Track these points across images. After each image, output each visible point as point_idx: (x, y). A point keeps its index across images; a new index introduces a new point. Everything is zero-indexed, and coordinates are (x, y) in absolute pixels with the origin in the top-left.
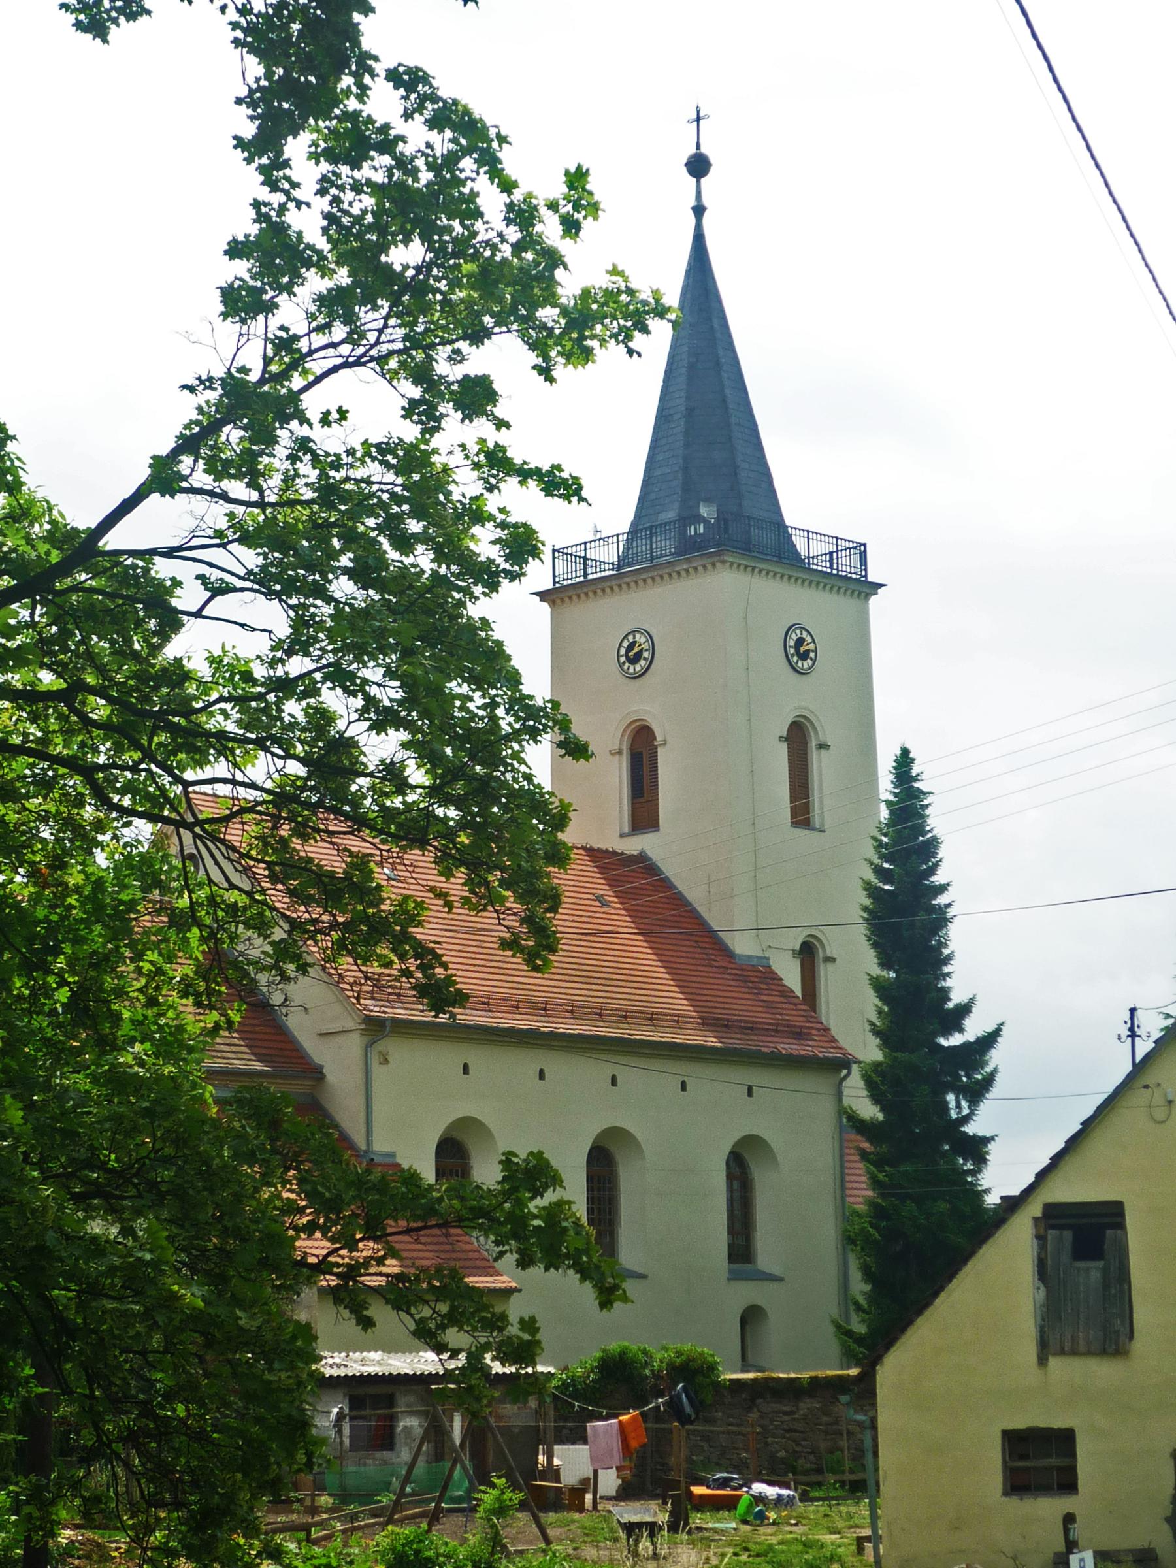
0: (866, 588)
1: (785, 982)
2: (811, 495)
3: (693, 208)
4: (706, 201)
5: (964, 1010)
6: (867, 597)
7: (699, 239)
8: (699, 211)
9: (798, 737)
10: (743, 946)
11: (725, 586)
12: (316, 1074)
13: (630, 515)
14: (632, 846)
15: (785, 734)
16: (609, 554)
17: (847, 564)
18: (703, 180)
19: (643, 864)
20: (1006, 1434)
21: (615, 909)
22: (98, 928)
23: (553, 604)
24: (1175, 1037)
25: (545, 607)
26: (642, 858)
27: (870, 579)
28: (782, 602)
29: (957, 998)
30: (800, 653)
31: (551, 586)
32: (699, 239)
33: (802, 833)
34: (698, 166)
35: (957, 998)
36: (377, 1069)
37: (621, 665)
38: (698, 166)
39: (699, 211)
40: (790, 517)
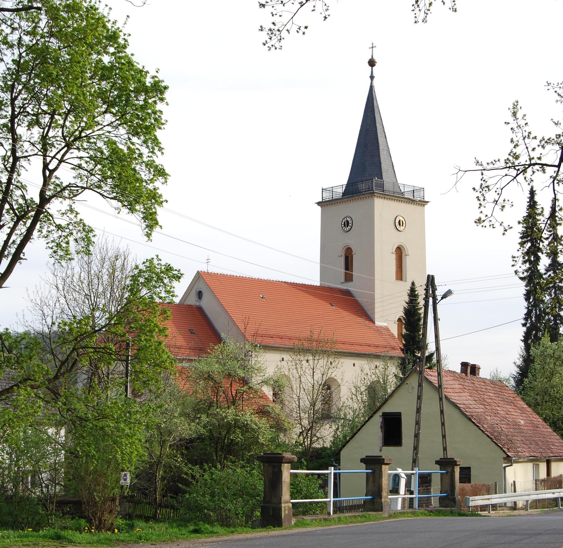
0: (423, 203)
1: (392, 331)
3: (198, 272)
4: (374, 74)
6: (424, 205)
7: (372, 87)
8: (372, 77)
9: (400, 252)
13: (345, 181)
14: (344, 287)
16: (341, 191)
18: (374, 68)
19: (348, 293)
20: (399, 414)
21: (557, 446)
22: (63, 452)
23: (321, 206)
25: (319, 208)
31: (321, 200)
32: (372, 87)
33: (400, 282)
37: (342, 228)
38: (372, 63)
39: (372, 77)
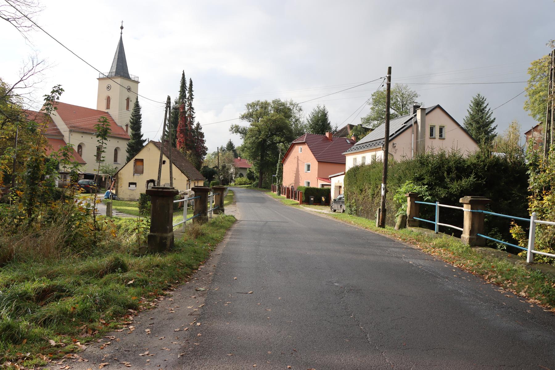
2: (132, 71)
5: (142, 136)
7: (121, 37)
8: (121, 33)
10: (119, 124)
11: (119, 80)
12: (63, 136)
14: (106, 111)
15: (63, 99)
17: (136, 79)
24: (2, 266)
26: (107, 113)
27: (384, 136)
28: (127, 83)
29: (142, 134)
30: (129, 89)
32: (121, 37)
34: (122, 28)
35: (142, 134)
36: (71, 136)
38: (122, 28)
39: (121, 33)
40: (129, 73)
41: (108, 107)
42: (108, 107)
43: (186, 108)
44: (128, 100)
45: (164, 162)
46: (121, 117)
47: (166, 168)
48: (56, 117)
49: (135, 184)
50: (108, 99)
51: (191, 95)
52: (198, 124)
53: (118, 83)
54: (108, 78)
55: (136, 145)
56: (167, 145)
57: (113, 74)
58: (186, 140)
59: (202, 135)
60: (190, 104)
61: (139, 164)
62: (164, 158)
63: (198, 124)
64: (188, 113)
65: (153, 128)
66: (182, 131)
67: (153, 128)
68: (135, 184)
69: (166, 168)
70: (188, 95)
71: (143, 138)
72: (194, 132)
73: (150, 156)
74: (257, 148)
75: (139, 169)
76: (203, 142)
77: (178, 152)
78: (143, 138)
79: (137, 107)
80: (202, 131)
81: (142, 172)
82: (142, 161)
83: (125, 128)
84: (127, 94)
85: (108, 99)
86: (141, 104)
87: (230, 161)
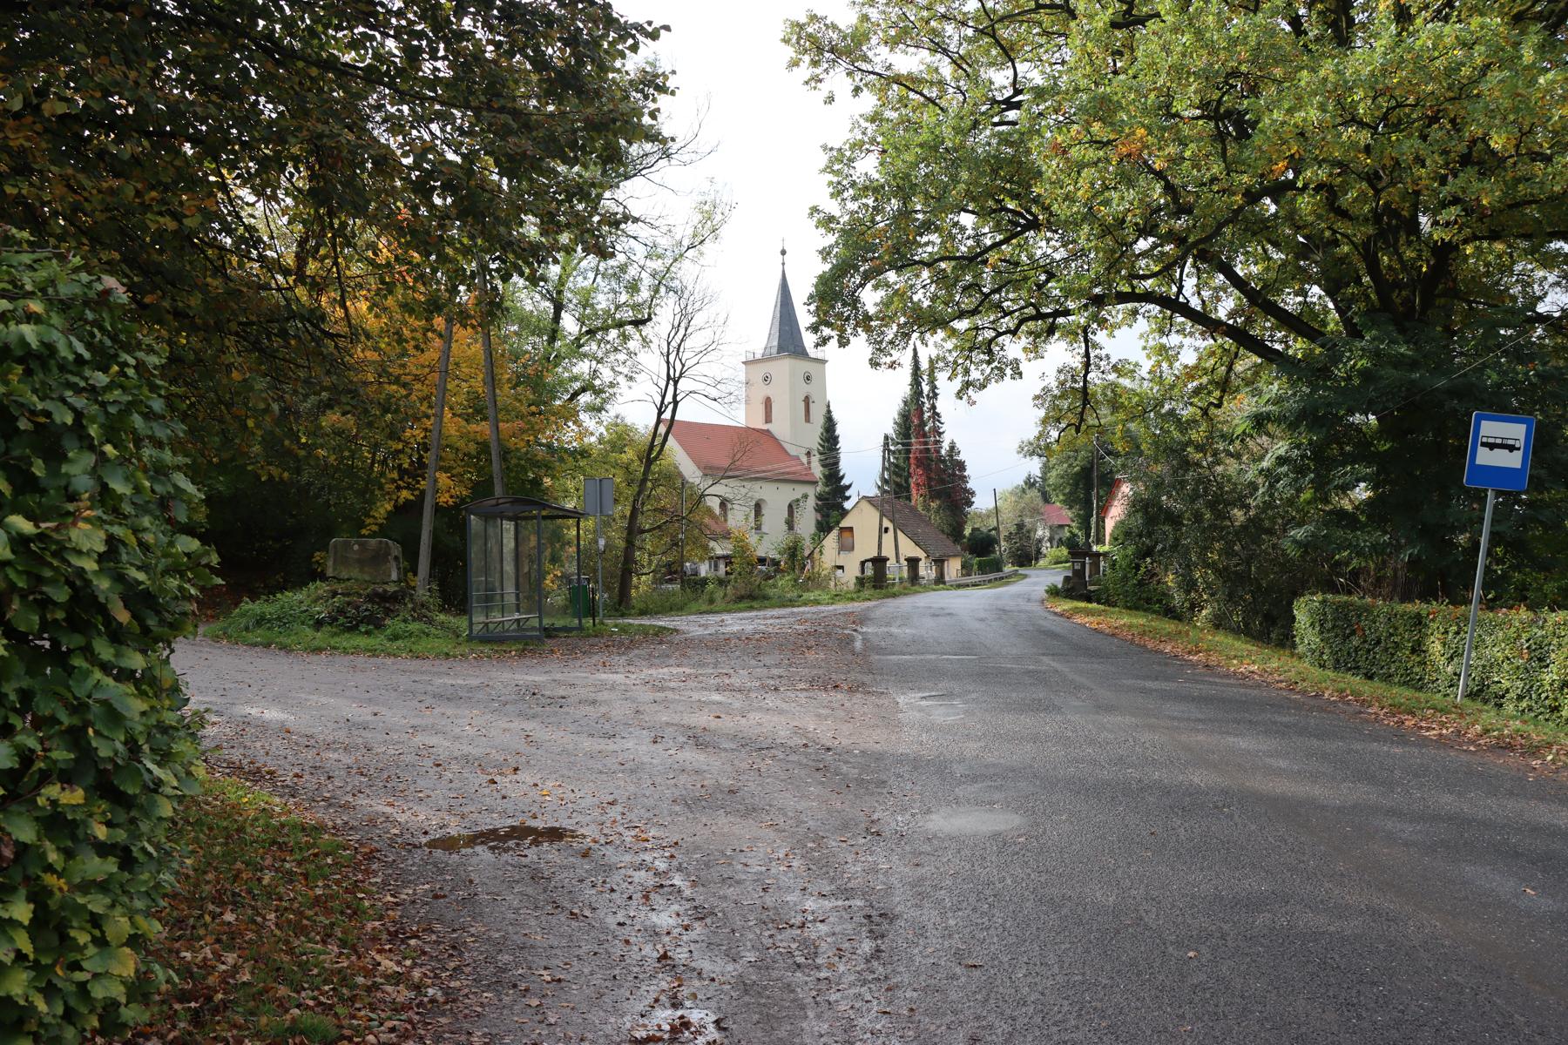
14: (765, 427)
28: (803, 366)
34: (783, 253)
38: (783, 253)
41: (768, 420)
42: (768, 420)
43: (927, 415)
44: (807, 400)
45: (886, 530)
46: (800, 439)
47: (888, 539)
48: (676, 454)
49: (841, 567)
50: (768, 403)
51: (934, 388)
52: (952, 447)
53: (785, 367)
54: (766, 359)
55: (833, 502)
56: (896, 484)
57: (775, 350)
58: (929, 479)
59: (961, 466)
60: (933, 407)
61: (846, 534)
62: (886, 523)
63: (952, 447)
64: (930, 424)
65: (863, 467)
66: (920, 463)
67: (863, 467)
68: (841, 567)
69: (888, 539)
70: (926, 389)
71: (845, 482)
72: (944, 461)
73: (864, 522)
74: (1076, 485)
75: (847, 541)
76: (964, 479)
77: (913, 509)
78: (845, 482)
79: (830, 425)
80: (961, 457)
81: (852, 549)
82: (851, 529)
83: (804, 459)
84: (805, 389)
85: (768, 403)
86: (836, 416)
87: (1035, 511)
